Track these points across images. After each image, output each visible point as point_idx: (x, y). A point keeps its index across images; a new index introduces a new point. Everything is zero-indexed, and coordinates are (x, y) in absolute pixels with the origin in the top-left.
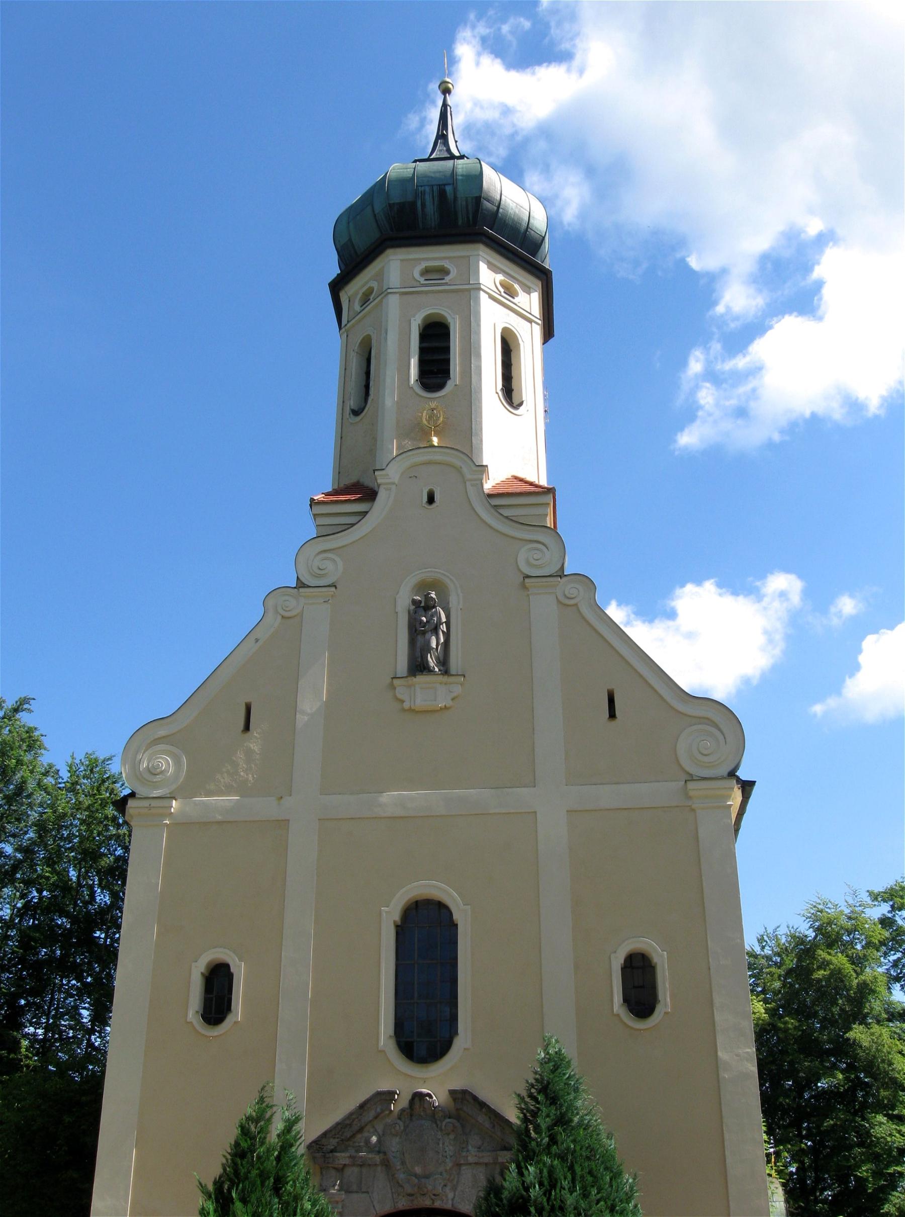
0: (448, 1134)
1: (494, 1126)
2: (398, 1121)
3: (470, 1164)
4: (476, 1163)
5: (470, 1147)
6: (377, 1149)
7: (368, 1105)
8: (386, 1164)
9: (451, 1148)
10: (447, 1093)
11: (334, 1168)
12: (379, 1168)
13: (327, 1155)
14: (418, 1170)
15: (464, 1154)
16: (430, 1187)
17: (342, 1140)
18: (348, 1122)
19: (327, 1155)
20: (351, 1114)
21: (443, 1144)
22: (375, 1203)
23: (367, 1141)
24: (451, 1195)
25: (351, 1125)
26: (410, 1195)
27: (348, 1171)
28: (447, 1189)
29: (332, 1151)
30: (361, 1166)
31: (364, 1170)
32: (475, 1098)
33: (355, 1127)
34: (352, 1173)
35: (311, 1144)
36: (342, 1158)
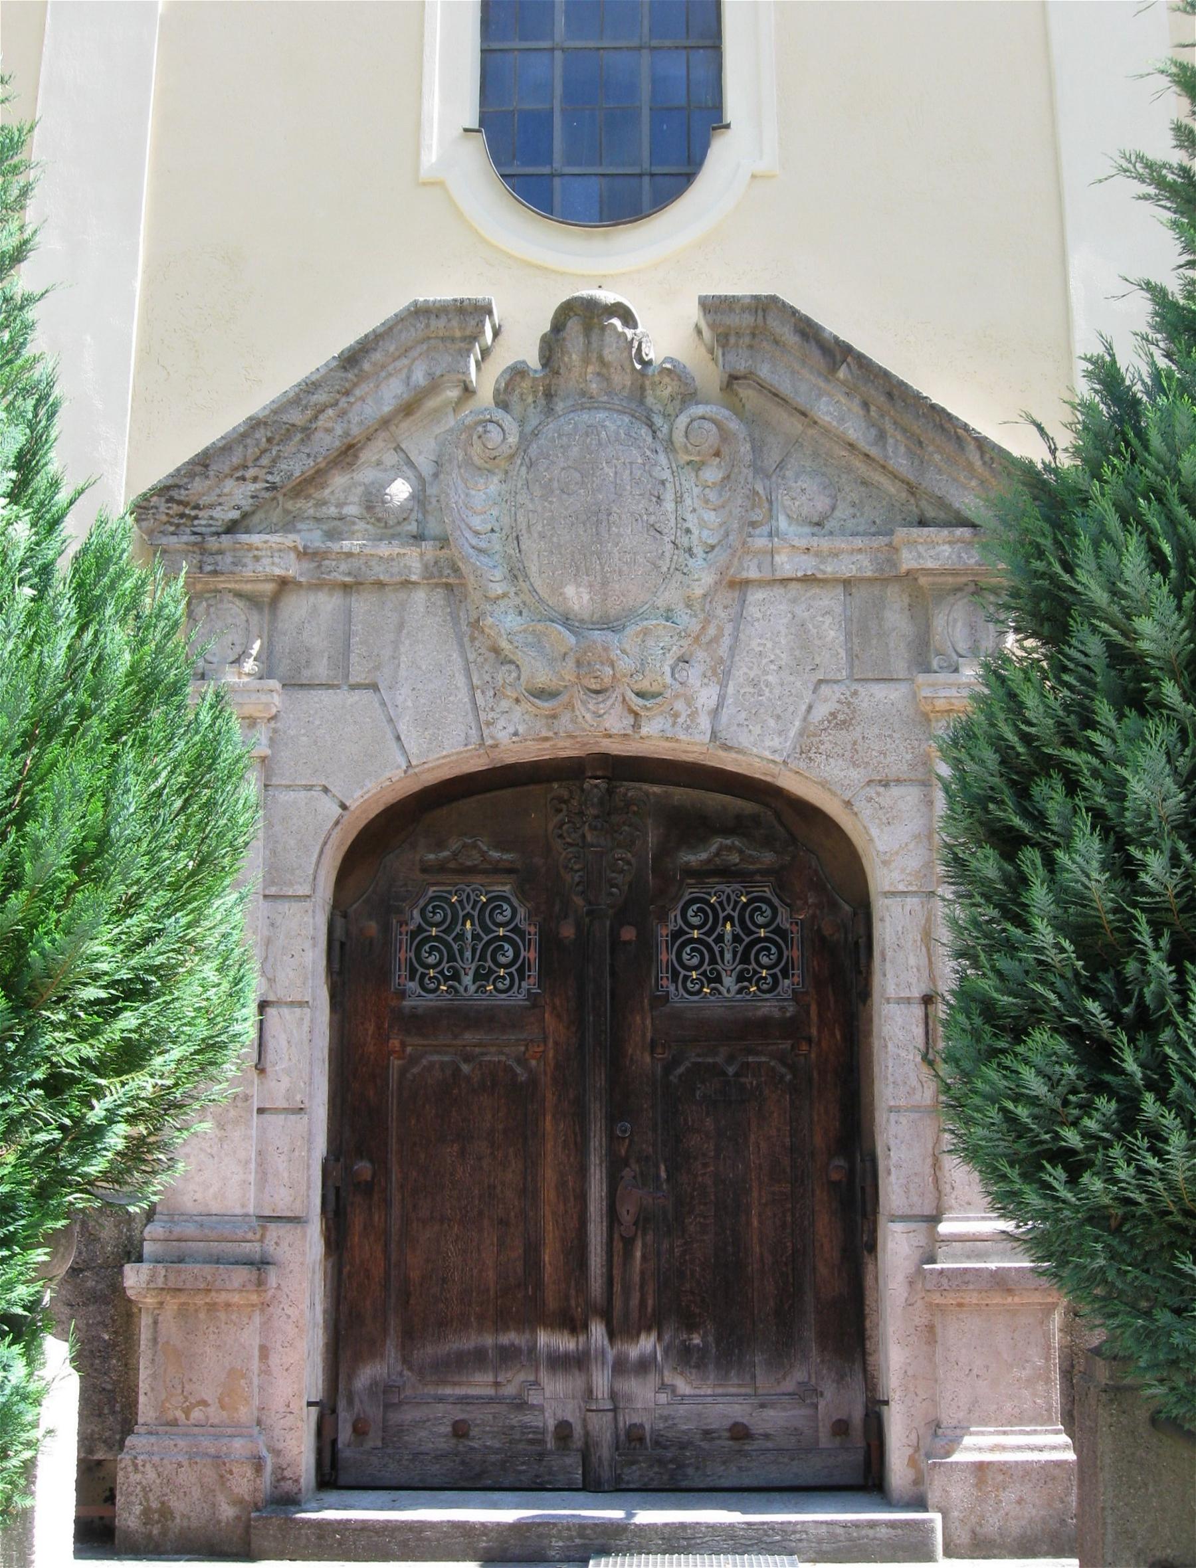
0: (697, 467)
1: (882, 436)
2: (499, 414)
3: (785, 581)
4: (808, 580)
5: (783, 523)
6: (412, 527)
7: (377, 356)
8: (449, 582)
9: (711, 517)
10: (693, 313)
11: (239, 595)
12: (420, 596)
13: (212, 543)
14: (577, 598)
15: (760, 542)
16: (625, 664)
17: (273, 487)
18: (296, 417)
19: (212, 543)
20: (310, 387)
21: (679, 500)
22: (402, 728)
23: (373, 501)
24: (707, 696)
25: (307, 432)
26: (542, 694)
27: (296, 608)
28: (693, 674)
29: (232, 528)
30: (346, 588)
31: (361, 604)
32: (808, 330)
33: (326, 442)
34: (310, 616)
35: (145, 497)
36: (271, 553)
